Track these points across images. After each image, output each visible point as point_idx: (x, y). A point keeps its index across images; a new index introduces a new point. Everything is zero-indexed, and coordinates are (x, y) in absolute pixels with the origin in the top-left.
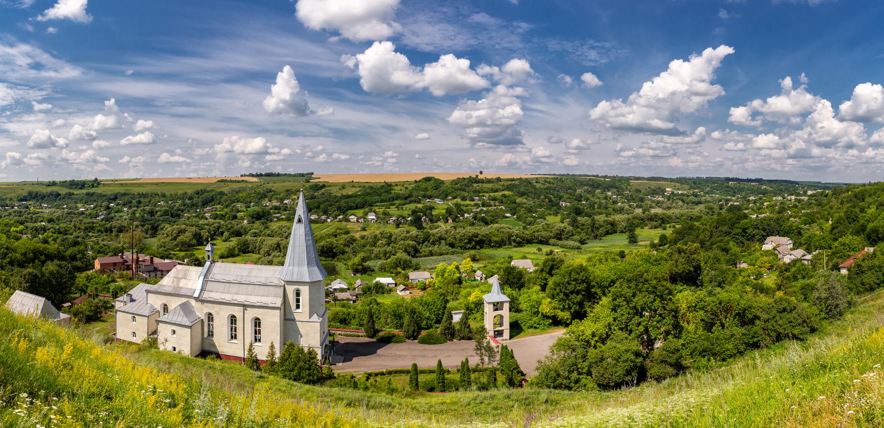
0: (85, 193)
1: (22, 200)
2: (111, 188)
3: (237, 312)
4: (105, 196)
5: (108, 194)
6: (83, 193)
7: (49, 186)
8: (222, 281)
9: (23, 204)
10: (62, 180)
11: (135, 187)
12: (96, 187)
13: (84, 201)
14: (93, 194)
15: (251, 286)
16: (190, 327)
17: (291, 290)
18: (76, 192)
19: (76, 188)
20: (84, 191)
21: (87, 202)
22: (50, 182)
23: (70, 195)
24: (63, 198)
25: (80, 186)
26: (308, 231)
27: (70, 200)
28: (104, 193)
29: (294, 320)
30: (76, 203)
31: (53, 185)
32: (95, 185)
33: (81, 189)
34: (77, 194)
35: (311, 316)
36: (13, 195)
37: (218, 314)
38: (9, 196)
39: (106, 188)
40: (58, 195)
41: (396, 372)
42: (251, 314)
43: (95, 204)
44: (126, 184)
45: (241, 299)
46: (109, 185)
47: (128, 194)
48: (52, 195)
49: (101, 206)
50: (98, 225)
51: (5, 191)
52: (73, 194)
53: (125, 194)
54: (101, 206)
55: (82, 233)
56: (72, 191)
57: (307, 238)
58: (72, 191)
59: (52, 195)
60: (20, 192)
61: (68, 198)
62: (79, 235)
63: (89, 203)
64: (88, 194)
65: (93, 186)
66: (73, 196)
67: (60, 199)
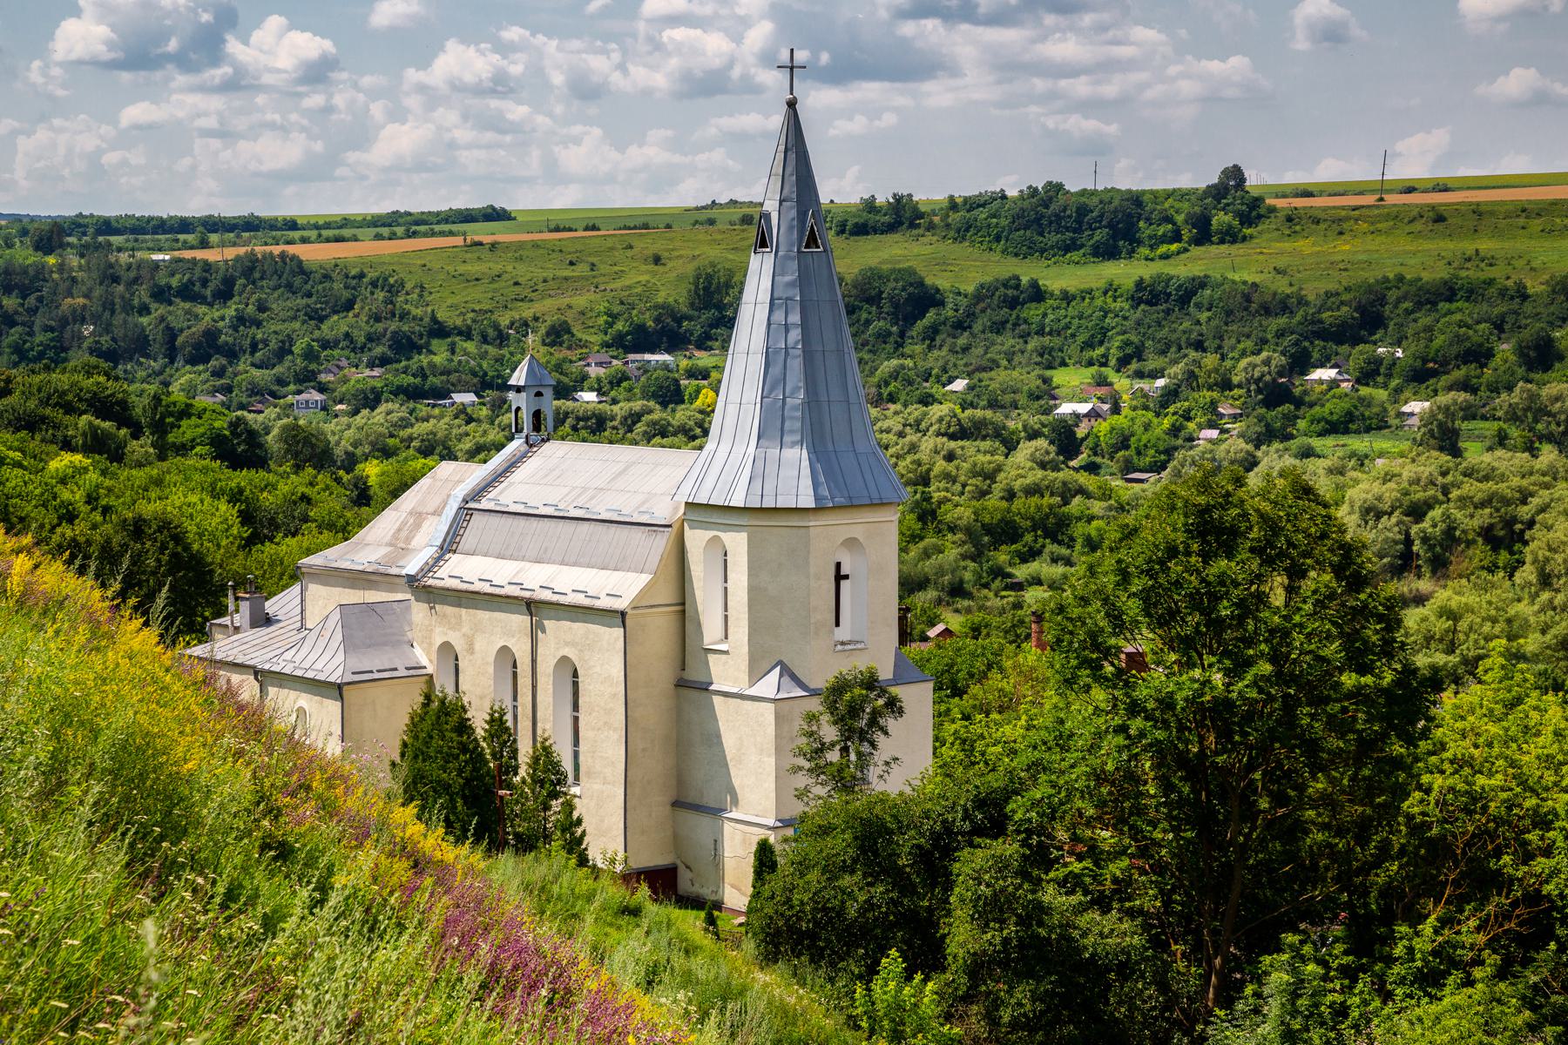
0: (1129, 284)
1: (641, 340)
2: (1343, 248)
3: (511, 629)
4: (1284, 306)
5: (1313, 290)
6: (1111, 289)
7: (861, 230)
8: (513, 508)
9: (645, 368)
10: (967, 188)
11: (1548, 232)
12: (1230, 236)
13: (1114, 347)
14: (1188, 293)
15: (586, 524)
16: (337, 690)
17: (696, 540)
18: (1060, 277)
19: (1068, 248)
20: (1126, 272)
21: (1139, 354)
22: (870, 205)
23: (1013, 303)
24: (960, 326)
25: (1100, 235)
26: (790, 285)
27: (1008, 341)
28: (1282, 286)
29: (704, 687)
30: (1051, 360)
31: (891, 228)
32: (1220, 219)
33: (1107, 252)
34: (1067, 298)
35: (756, 675)
36: (580, 301)
37: (471, 650)
38: (547, 308)
39: (1306, 246)
40: (921, 299)
41: (576, 685)
42: (560, 638)
43: (1177, 370)
44: (1478, 211)
45: (537, 578)
46: (1337, 224)
47: (1473, 293)
48: (874, 300)
49: (1226, 385)
50: (1097, 507)
51: (523, 272)
52: (1037, 294)
53: (1448, 292)
54: (1226, 385)
55: (951, 554)
56: (1028, 271)
57: (779, 316)
58: (1028, 271)
59: (874, 300)
60: (637, 276)
61: (998, 328)
62: (929, 566)
63: (1152, 363)
64: (1148, 294)
65: (1203, 234)
66: (1032, 312)
67: (931, 335)
